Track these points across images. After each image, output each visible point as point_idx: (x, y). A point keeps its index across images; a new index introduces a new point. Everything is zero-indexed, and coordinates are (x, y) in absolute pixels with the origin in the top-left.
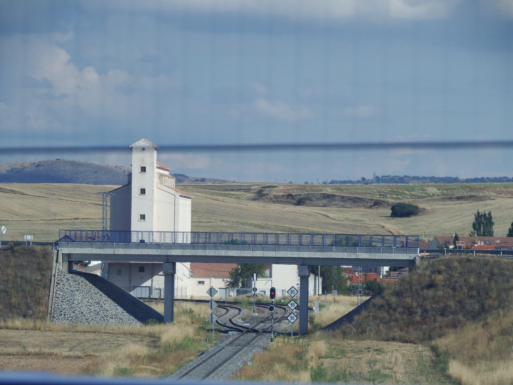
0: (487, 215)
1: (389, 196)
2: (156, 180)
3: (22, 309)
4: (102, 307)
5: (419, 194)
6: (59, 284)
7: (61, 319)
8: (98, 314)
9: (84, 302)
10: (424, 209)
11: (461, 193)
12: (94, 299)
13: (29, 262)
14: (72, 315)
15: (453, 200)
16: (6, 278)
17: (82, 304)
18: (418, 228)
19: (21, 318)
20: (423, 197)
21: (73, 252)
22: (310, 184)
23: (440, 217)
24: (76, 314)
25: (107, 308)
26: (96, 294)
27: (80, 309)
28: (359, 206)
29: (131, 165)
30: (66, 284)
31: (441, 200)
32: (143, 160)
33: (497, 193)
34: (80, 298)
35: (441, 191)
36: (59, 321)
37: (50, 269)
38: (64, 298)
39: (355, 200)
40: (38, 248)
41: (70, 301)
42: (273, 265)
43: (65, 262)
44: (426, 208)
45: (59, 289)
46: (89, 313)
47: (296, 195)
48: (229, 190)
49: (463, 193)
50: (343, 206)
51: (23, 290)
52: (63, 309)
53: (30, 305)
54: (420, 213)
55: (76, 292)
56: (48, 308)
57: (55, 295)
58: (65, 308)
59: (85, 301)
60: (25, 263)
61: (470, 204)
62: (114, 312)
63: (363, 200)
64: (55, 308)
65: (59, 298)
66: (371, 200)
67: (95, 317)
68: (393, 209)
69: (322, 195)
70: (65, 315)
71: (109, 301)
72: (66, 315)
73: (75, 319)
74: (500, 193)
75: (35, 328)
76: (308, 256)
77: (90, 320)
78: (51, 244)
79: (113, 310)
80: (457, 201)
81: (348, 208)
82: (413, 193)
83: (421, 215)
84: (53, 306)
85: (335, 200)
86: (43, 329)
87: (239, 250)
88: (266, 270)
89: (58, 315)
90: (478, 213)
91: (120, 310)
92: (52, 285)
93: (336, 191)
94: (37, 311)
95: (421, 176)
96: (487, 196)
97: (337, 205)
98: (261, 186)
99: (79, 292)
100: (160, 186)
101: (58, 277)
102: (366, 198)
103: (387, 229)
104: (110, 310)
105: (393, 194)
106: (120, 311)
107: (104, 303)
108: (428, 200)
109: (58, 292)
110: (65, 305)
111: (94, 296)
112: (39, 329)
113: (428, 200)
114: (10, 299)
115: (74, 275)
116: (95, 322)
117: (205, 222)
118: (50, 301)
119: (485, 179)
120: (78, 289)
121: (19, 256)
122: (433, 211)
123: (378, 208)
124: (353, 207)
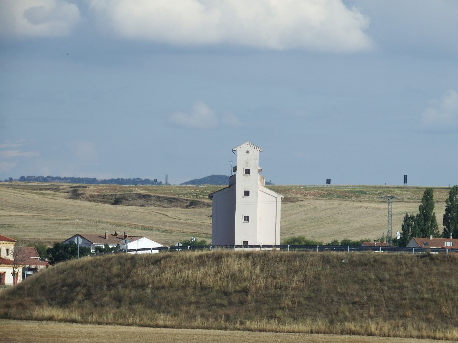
1: (201, 196)
16: (431, 287)
32: (247, 163)
39: (171, 200)
47: (112, 194)
48: (38, 189)
50: (160, 206)
60: (448, 271)
66: (187, 200)
69: (137, 195)
74: (305, 195)
81: (165, 207)
85: (151, 200)
90: (407, 215)
95: (62, 177)
97: (154, 205)
98: (69, 186)
102: (181, 199)
114: (441, 308)
119: (121, 180)
124: (170, 206)
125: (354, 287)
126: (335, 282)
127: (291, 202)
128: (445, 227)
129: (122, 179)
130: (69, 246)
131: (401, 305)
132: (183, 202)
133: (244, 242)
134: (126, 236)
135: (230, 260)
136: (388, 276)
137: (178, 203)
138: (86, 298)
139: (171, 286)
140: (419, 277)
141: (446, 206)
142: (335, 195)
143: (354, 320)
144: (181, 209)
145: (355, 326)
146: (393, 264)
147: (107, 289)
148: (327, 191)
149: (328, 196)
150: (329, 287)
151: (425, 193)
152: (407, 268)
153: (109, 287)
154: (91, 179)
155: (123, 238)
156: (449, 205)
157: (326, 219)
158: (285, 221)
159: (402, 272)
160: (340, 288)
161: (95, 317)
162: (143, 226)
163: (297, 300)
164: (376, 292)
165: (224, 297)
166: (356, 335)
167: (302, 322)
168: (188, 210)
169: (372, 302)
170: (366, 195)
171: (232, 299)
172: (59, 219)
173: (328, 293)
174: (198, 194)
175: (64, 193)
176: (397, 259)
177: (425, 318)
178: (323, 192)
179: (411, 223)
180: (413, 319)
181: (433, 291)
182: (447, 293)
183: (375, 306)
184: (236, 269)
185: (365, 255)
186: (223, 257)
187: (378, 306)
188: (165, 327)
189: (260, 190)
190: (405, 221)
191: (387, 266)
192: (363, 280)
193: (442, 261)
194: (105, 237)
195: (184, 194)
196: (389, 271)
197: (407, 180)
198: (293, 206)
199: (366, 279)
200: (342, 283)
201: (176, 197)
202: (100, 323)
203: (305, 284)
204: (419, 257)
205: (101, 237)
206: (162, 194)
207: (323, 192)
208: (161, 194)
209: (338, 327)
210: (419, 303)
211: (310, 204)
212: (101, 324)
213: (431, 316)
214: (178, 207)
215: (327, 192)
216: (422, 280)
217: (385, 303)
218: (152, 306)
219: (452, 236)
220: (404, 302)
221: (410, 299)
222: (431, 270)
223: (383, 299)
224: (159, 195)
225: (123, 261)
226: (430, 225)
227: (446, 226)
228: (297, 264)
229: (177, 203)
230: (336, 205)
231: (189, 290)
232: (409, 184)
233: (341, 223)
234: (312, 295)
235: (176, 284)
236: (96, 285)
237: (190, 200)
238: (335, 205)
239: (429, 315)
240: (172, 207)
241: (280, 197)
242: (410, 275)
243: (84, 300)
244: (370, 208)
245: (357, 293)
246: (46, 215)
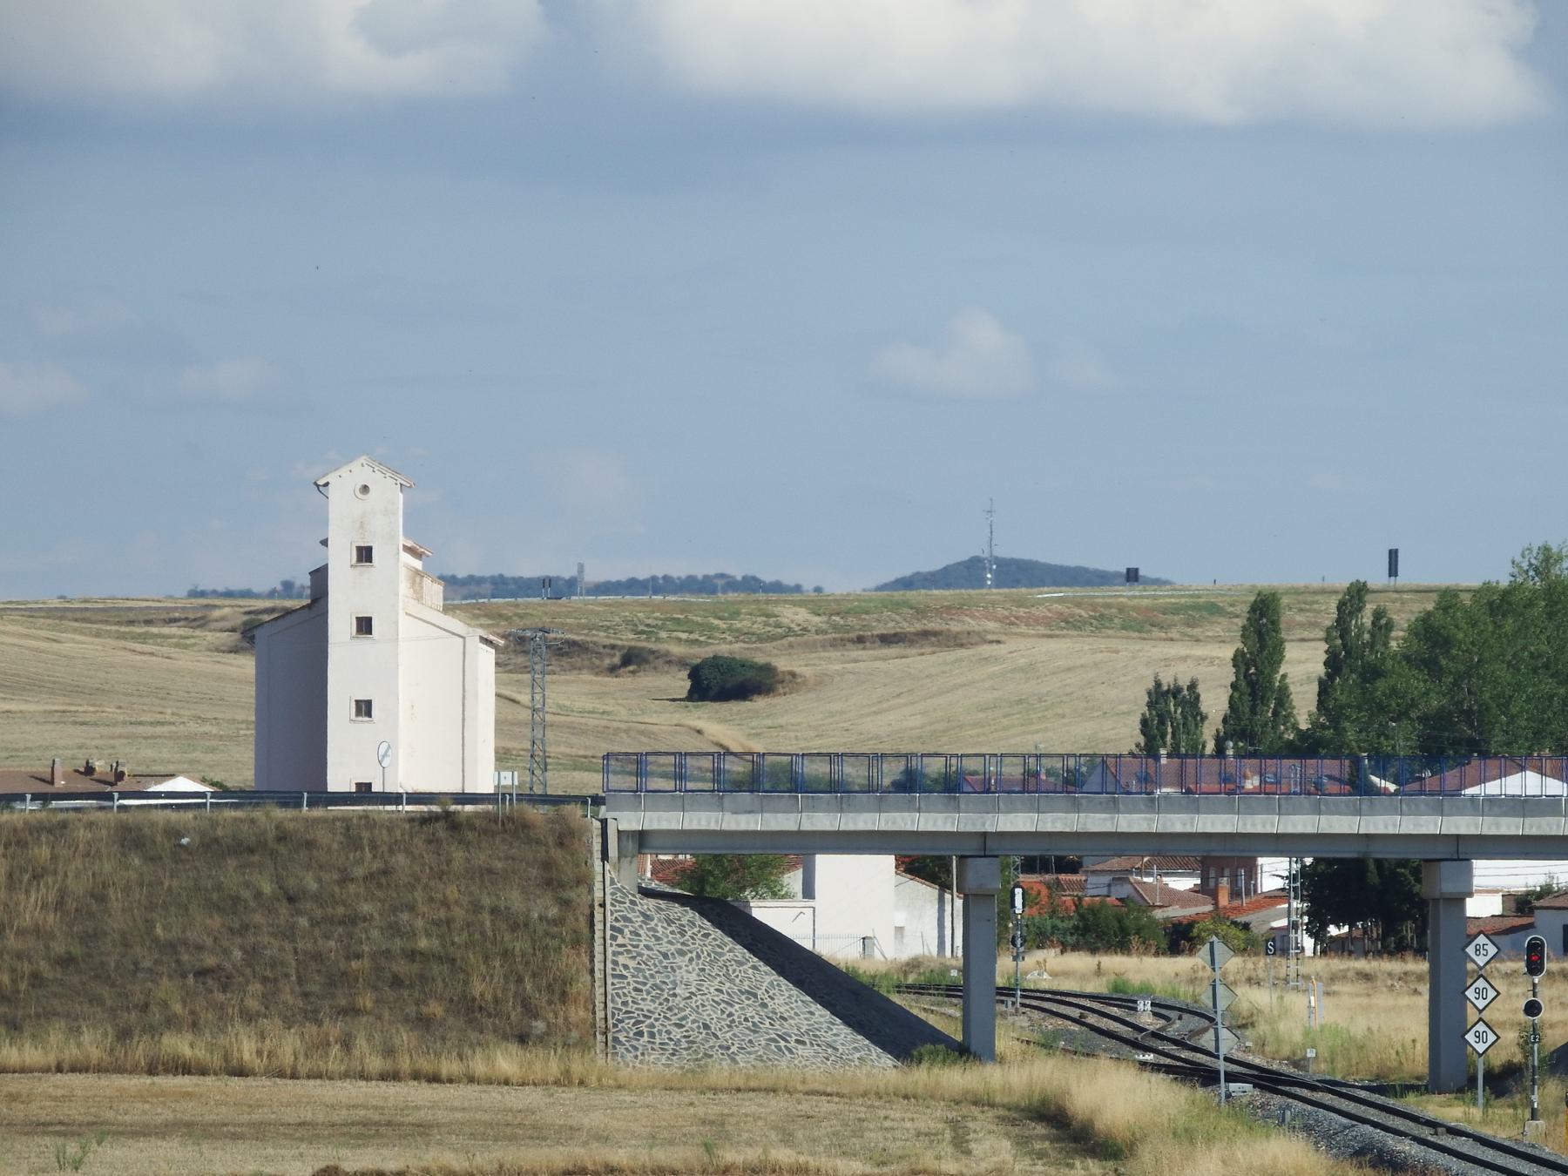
0: (1185, 692)
1: (663, 635)
2: (404, 588)
3: (509, 1018)
4: (764, 1005)
5: (758, 627)
6: (620, 931)
7: (640, 1048)
8: (755, 1029)
9: (706, 991)
10: (793, 675)
11: (891, 624)
12: (737, 981)
13: (513, 859)
14: (677, 1034)
15: (868, 644)
16: (442, 914)
17: (704, 997)
18: (792, 735)
19: (514, 1048)
20: (773, 638)
21: (655, 826)
22: (813, 595)
23: (847, 700)
24: (687, 1031)
25: (782, 1010)
26: (740, 963)
27: (698, 1013)
28: (575, 669)
29: (325, 543)
30: (641, 932)
32: (362, 526)
33: (1001, 622)
34: (693, 977)
35: (824, 618)
36: (636, 1057)
37: (584, 881)
38: (641, 980)
40: (537, 813)
41: (664, 987)
42: (818, 857)
43: (629, 859)
44: (797, 670)
45: (621, 949)
46: (729, 1026)
48: (139, 622)
49: (898, 623)
51: (506, 954)
52: (645, 1016)
53: (533, 1001)
54: (780, 686)
55: (679, 959)
56: (594, 1013)
57: (614, 969)
58: (649, 1011)
59: (711, 987)
61: (929, 657)
62: (806, 1022)
63: (587, 649)
64: (616, 1012)
65: (626, 977)
66: (613, 647)
67: (747, 1040)
68: (695, 674)
70: (652, 1035)
71: (783, 988)
72: (657, 1036)
73: (685, 1049)
74: (1012, 624)
75: (564, 1080)
76: (1473, 831)
77: (734, 1049)
78: (582, 800)
79: (802, 1016)
80: (880, 647)
82: (737, 624)
83: (785, 694)
84: (610, 1005)
86: (594, 1084)
87: (1561, 816)
88: (783, 873)
89: (631, 1035)
90: (1158, 684)
91: (821, 1016)
92: (598, 935)
93: (490, 622)
94: (560, 1021)
96: (974, 631)
97: (506, 665)
99: (687, 958)
100: (415, 608)
101: (613, 909)
104: (791, 1018)
105: (676, 628)
106: (822, 1020)
107: (771, 994)
108: (791, 646)
109: (621, 960)
110: (648, 1002)
111: (734, 971)
112: (582, 1083)
113: (791, 646)
114: (466, 983)
115: (661, 902)
116: (753, 1056)
117: (152, 724)
118: (599, 991)
119: (661, 582)
120: (684, 948)
121: (479, 842)
122: (822, 681)
125: (208, 921)
126: (151, 907)
127: (962, 646)
129: (665, 578)
131: (344, 974)
132: (600, 653)
133: (358, 785)
134: (122, 773)
136: (313, 886)
137: (585, 657)
140: (409, 883)
141: (1326, 652)
142: (1116, 621)
143: (195, 1026)
145: (191, 1046)
146: (335, 846)
149: (1091, 624)
150: (131, 924)
152: (375, 857)
154: (563, 579)
155: (112, 779)
156: (1335, 647)
159: (359, 872)
160: (164, 928)
163: (26, 968)
164: (273, 934)
166: (194, 1074)
167: (34, 1036)
168: (615, 679)
169: (257, 968)
170: (1221, 619)
172: (133, 720)
173: (126, 945)
174: (654, 627)
175: (218, 634)
176: (348, 829)
177: (414, 1014)
178: (1077, 611)
179: (1172, 709)
180: (379, 1017)
181: (449, 927)
182: (490, 933)
183: (265, 980)
185: (253, 821)
187: (276, 980)
189: (410, 615)
190: (1150, 705)
191: (315, 852)
192: (236, 900)
193: (486, 832)
194: (49, 778)
196: (321, 867)
197: (1399, 559)
198: (962, 660)
199: (246, 894)
200: (173, 909)
203: (61, 917)
204: (416, 824)
205: (37, 778)
207: (1077, 611)
209: (140, 1049)
210: (401, 967)
213: (435, 1008)
214: (585, 671)
216: (419, 895)
217: (298, 972)
220: (354, 964)
221: (373, 956)
222: (449, 862)
223: (290, 959)
226: (1270, 715)
228: (43, 852)
229: (579, 660)
232: (1406, 577)
234: (77, 950)
237: (621, 648)
239: (428, 1005)
242: (383, 881)
244: (1212, 663)
245: (215, 939)
246: (91, 709)
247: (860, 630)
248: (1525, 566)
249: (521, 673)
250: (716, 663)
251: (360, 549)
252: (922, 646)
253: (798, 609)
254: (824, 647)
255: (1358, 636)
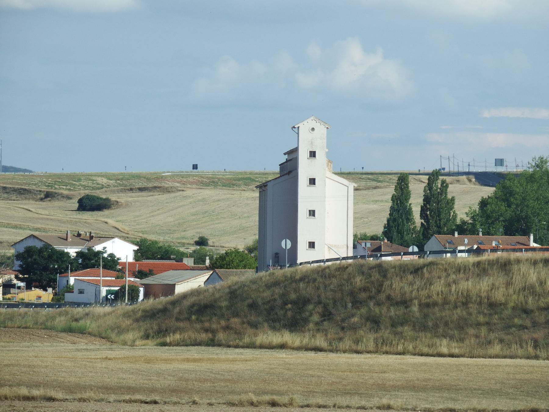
10: (117, 202)
15: (134, 191)
28: (27, 199)
31: (121, 191)
32: (312, 143)
39: (20, 192)
44: (118, 200)
49: (142, 183)
50: (8, 199)
63: (31, 192)
66: (40, 191)
81: (14, 200)
96: (173, 187)
103: (112, 225)
113: (106, 191)
122: (127, 205)
123: (51, 201)
124: (20, 199)
128: (423, 221)
130: (45, 250)
132: (36, 193)
134: (93, 236)
135: (524, 268)
137: (29, 194)
138: (323, 319)
139: (446, 302)
142: (219, 183)
144: (34, 202)
147: (352, 306)
148: (208, 178)
151: (399, 180)
153: (357, 303)
155: (89, 239)
157: (221, 213)
158: (172, 216)
161: (347, 343)
162: (8, 224)
165: (524, 316)
171: (537, 319)
174: (52, 184)
184: (535, 279)
186: (512, 264)
188: (452, 356)
194: (65, 238)
195: (35, 184)
201: (26, 187)
202: (358, 352)
205: (60, 238)
206: (8, 184)
208: (8, 185)
211: (195, 195)
212: (361, 353)
215: (209, 180)
218: (424, 328)
219: (481, 233)
224: (5, 186)
225: (365, 269)
227: (424, 219)
229: (28, 195)
230: (228, 195)
231: (473, 308)
233: (240, 217)
235: (452, 298)
236: (335, 302)
237: (44, 191)
238: (228, 196)
240: (23, 199)
241: (352, 185)
243: (322, 321)
247: (129, 186)
248: (534, 164)
249: (7, 200)
250: (87, 197)
251: (311, 152)
252: (154, 192)
253: (103, 178)
254: (118, 192)
255: (436, 190)
